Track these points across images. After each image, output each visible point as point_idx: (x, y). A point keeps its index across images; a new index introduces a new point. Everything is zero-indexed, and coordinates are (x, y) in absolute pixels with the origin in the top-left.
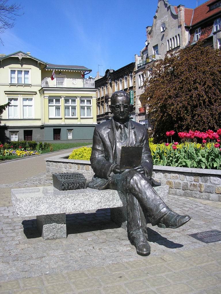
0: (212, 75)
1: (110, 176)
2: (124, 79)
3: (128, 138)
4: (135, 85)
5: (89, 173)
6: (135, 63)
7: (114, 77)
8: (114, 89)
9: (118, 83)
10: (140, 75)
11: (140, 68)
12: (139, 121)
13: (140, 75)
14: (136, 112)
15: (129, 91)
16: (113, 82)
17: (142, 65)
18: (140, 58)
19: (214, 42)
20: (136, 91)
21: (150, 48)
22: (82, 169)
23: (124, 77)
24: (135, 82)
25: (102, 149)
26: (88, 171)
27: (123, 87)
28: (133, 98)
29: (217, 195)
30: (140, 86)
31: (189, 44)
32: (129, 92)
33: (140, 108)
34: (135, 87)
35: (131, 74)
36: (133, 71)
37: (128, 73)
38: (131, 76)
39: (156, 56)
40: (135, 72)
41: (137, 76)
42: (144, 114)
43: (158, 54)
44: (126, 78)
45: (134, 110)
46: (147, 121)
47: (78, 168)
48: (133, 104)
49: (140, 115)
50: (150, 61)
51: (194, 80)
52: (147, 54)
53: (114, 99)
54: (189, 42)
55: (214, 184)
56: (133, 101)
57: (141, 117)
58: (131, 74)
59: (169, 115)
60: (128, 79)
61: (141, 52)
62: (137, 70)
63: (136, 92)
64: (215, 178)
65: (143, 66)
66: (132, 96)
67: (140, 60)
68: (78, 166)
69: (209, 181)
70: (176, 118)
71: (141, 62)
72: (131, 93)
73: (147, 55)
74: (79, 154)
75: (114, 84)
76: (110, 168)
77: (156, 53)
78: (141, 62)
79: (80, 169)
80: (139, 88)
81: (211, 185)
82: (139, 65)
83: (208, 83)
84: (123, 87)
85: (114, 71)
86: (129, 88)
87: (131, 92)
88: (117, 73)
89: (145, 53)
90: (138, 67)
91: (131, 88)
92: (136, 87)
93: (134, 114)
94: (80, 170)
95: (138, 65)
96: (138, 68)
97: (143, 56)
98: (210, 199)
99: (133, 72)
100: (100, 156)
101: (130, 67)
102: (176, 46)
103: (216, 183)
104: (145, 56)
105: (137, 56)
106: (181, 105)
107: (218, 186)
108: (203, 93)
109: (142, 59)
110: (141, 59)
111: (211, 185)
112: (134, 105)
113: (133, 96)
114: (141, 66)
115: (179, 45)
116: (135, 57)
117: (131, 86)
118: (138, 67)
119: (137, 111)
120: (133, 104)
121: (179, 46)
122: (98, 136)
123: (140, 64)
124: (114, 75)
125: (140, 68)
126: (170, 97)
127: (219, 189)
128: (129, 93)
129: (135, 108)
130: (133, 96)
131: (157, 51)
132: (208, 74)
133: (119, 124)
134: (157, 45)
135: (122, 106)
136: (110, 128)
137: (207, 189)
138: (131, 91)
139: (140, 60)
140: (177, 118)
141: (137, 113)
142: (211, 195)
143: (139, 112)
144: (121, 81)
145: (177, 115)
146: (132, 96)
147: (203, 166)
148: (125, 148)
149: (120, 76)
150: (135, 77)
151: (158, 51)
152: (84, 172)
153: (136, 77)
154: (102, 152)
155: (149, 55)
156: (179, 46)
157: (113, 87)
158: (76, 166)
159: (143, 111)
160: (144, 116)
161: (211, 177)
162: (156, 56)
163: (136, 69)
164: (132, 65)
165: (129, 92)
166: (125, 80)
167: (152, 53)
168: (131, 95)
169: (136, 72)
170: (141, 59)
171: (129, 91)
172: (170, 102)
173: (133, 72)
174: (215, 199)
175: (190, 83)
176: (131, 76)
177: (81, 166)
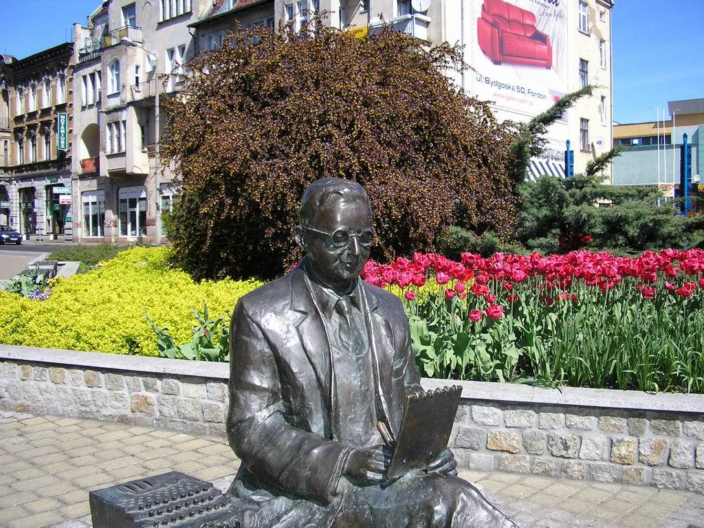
0: (366, 104)
1: (335, 494)
2: (42, 85)
3: (367, 345)
4: (72, 100)
5: (65, 392)
6: (72, 44)
7: (15, 76)
8: (13, 109)
9: (26, 92)
10: (85, 77)
11: (86, 58)
12: (82, 193)
13: (85, 77)
14: (73, 170)
15: (55, 116)
16: (11, 89)
17: (93, 52)
18: (88, 33)
19: (276, 13)
20: (74, 117)
21: (116, 11)
22: (39, 378)
23: (43, 78)
24: (71, 93)
25: (274, 385)
26: (60, 386)
27: (40, 102)
28: (65, 136)
29: (491, 456)
30: (84, 104)
31: (214, 11)
32: (56, 119)
33: (83, 161)
34: (71, 105)
35: (61, 72)
36: (68, 63)
37: (52, 68)
38: (63, 78)
39: (131, 30)
40: (72, 67)
41: (78, 77)
42: (95, 175)
43: (135, 27)
44: (48, 82)
45: (69, 165)
46: (102, 192)
47: (25, 375)
48: (66, 150)
49: (83, 177)
50: (114, 42)
51: (319, 116)
52: (104, 25)
53: (325, 211)
54: (214, 5)
55: (484, 425)
56: (65, 141)
57: (87, 183)
58: (61, 72)
59: (254, 205)
60: (52, 83)
61: (90, 18)
62: (78, 62)
63: (75, 119)
64: (486, 409)
65: (95, 55)
66: (63, 127)
67: (87, 38)
68: (23, 369)
69: (468, 416)
70: (272, 213)
71: (89, 43)
72: (60, 122)
73: (107, 27)
74: (7, 322)
75: (14, 94)
76: (338, 464)
77: (128, 24)
78: (88, 45)
79: (32, 377)
80: (84, 108)
81: (473, 427)
82: (84, 52)
83: (359, 126)
84: (40, 102)
85: (14, 59)
86: (54, 108)
87: (60, 119)
88: (25, 67)
89: (100, 21)
90: (80, 54)
91: (61, 108)
92: (74, 106)
93: (68, 174)
94: (32, 383)
95: (81, 50)
96: (80, 58)
97: (94, 29)
98: (471, 465)
99: (68, 68)
100: (265, 413)
101: (61, 54)
102: (181, 12)
103: (490, 421)
104: (100, 29)
105: (78, 27)
106: (285, 179)
107: (494, 430)
108: (347, 151)
109: (92, 35)
110: (88, 37)
111: (473, 427)
112: (69, 151)
113: (65, 130)
114: (87, 54)
115: (189, 10)
116: (75, 29)
117: (60, 102)
118: (82, 56)
119: (76, 168)
120: (66, 150)
121: (190, 14)
122: (257, 337)
123: (87, 47)
124: (15, 70)
125: (86, 58)
126: (255, 155)
127: (498, 437)
128: (54, 121)
129: (70, 160)
130: (65, 130)
131: (133, 20)
132: (357, 101)
133: (335, 297)
134: (132, 6)
135: (357, 237)
136: (302, 309)
137: (463, 439)
138: (62, 116)
139: (87, 38)
140: (274, 212)
141: (76, 173)
142: (474, 455)
143: (80, 171)
144: (34, 87)
145: (274, 207)
146: (63, 127)
147: (430, 367)
148: (416, 400)
149: (33, 75)
150: (71, 80)
151: (134, 19)
152: (47, 387)
153: (74, 81)
154: (274, 396)
155: (111, 28)
156: (190, 14)
157: (12, 103)
158: (18, 369)
159: (91, 168)
160: (95, 182)
161: (475, 408)
162: (131, 30)
163: (76, 60)
164: (66, 49)
165: (56, 119)
166: (45, 86)
167: (120, 23)
168: (61, 125)
169: (76, 69)
170: (88, 37)
171: (55, 116)
172: (257, 168)
173: (68, 68)
174: (484, 466)
175: (309, 121)
176: (63, 78)
177: (34, 371)
